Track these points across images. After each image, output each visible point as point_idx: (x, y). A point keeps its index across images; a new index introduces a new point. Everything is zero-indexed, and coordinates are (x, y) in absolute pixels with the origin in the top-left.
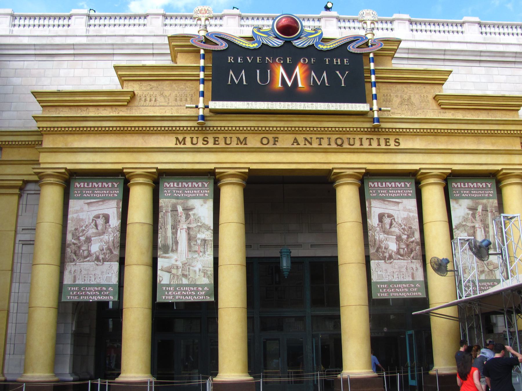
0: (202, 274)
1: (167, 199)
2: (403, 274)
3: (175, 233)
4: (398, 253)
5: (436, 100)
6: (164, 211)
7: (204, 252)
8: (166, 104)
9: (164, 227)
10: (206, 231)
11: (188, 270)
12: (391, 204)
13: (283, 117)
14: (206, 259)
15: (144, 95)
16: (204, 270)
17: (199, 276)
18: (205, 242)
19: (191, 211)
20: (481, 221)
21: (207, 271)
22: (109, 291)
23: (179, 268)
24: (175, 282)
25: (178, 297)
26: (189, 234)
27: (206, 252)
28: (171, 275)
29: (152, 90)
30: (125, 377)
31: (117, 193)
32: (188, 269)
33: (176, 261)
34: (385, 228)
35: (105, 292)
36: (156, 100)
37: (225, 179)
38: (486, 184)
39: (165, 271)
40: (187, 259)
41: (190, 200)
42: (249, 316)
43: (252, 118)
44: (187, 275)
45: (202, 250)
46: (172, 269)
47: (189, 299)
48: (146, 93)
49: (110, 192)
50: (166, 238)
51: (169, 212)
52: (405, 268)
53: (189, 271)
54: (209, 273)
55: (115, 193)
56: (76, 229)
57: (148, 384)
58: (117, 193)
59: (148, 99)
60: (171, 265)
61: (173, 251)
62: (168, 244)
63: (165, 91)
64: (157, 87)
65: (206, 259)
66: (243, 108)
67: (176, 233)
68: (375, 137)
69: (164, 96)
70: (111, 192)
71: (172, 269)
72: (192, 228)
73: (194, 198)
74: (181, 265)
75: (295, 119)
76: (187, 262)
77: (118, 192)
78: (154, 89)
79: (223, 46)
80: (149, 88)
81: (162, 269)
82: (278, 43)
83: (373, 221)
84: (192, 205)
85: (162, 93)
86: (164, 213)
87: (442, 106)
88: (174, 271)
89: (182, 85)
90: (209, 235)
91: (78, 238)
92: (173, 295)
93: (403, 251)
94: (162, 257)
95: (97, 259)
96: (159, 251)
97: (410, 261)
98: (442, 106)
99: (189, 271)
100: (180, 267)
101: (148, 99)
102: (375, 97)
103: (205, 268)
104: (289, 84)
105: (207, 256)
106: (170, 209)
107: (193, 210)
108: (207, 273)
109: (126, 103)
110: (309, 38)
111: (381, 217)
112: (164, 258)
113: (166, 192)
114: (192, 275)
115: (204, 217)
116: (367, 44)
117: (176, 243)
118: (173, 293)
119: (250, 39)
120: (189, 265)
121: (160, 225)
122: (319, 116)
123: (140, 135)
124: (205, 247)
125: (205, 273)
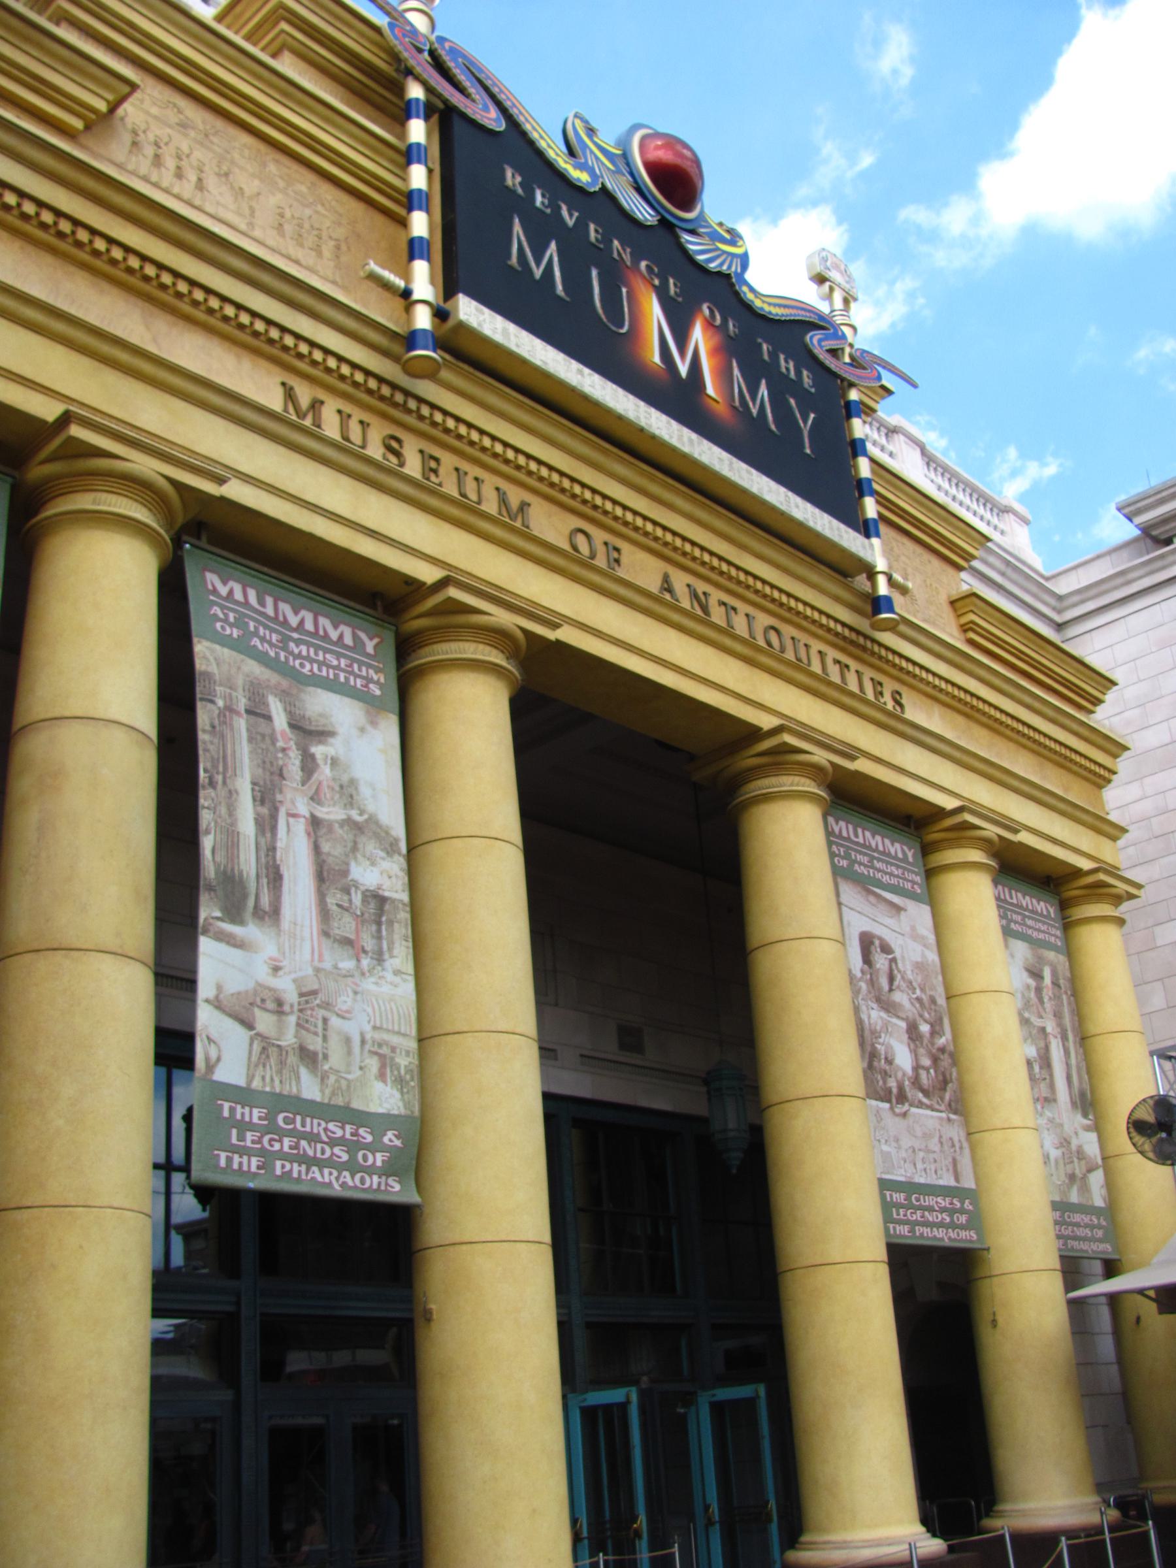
0: (373, 1064)
1: (226, 651)
2: (935, 1161)
3: (267, 825)
4: (916, 1082)
5: (955, 610)
6: (221, 703)
7: (379, 958)
8: (243, 227)
9: (224, 783)
10: (383, 854)
11: (320, 1030)
12: (882, 907)
13: (652, 479)
14: (386, 989)
16: (380, 1045)
17: (361, 1068)
18: (380, 911)
19: (320, 742)
20: (1055, 1016)
21: (393, 1049)
22: (384, 1148)
23: (287, 1008)
24: (265, 1082)
25: (283, 1166)
26: (317, 849)
27: (386, 956)
28: (252, 1040)
30: (844, 1545)
31: (377, 683)
32: (320, 1024)
33: (276, 969)
34: (880, 989)
37: (435, 647)
39: (230, 1015)
40: (317, 970)
41: (311, 689)
42: (163, 1371)
43: (562, 437)
44: (315, 1054)
45: (369, 943)
46: (257, 1011)
47: (324, 1184)
48: (161, 132)
49: (351, 666)
50: (232, 839)
51: (238, 713)
52: (936, 1139)
53: (325, 1038)
54: (403, 1061)
57: (1104, 1534)
58: (377, 683)
59: (170, 163)
60: (251, 985)
61: (259, 914)
62: (241, 873)
63: (237, 170)
65: (386, 989)
66: (568, 380)
67: (274, 829)
69: (232, 188)
71: (257, 1011)
72: (330, 825)
73: (331, 686)
74: (291, 996)
75: (679, 502)
76: (316, 987)
80: (173, 118)
81: (217, 997)
84: (321, 715)
85: (225, 168)
86: (221, 713)
87: (972, 635)
88: (265, 1022)
89: (302, 183)
90: (394, 879)
92: (262, 1153)
93: (928, 1079)
94: (222, 937)
96: (204, 898)
97: (943, 1115)
98: (972, 635)
99: (325, 1038)
100: (292, 1006)
103: (386, 1036)
105: (389, 976)
106: (242, 703)
107: (331, 740)
108: (392, 1059)
109: (78, 124)
110: (717, 249)
112: (228, 943)
113: (221, 616)
114: (336, 1059)
115: (374, 789)
117: (275, 877)
118: (260, 1141)
120: (327, 1006)
121: (209, 765)
122: (741, 521)
123: (133, 299)
124: (379, 931)
125: (382, 1057)
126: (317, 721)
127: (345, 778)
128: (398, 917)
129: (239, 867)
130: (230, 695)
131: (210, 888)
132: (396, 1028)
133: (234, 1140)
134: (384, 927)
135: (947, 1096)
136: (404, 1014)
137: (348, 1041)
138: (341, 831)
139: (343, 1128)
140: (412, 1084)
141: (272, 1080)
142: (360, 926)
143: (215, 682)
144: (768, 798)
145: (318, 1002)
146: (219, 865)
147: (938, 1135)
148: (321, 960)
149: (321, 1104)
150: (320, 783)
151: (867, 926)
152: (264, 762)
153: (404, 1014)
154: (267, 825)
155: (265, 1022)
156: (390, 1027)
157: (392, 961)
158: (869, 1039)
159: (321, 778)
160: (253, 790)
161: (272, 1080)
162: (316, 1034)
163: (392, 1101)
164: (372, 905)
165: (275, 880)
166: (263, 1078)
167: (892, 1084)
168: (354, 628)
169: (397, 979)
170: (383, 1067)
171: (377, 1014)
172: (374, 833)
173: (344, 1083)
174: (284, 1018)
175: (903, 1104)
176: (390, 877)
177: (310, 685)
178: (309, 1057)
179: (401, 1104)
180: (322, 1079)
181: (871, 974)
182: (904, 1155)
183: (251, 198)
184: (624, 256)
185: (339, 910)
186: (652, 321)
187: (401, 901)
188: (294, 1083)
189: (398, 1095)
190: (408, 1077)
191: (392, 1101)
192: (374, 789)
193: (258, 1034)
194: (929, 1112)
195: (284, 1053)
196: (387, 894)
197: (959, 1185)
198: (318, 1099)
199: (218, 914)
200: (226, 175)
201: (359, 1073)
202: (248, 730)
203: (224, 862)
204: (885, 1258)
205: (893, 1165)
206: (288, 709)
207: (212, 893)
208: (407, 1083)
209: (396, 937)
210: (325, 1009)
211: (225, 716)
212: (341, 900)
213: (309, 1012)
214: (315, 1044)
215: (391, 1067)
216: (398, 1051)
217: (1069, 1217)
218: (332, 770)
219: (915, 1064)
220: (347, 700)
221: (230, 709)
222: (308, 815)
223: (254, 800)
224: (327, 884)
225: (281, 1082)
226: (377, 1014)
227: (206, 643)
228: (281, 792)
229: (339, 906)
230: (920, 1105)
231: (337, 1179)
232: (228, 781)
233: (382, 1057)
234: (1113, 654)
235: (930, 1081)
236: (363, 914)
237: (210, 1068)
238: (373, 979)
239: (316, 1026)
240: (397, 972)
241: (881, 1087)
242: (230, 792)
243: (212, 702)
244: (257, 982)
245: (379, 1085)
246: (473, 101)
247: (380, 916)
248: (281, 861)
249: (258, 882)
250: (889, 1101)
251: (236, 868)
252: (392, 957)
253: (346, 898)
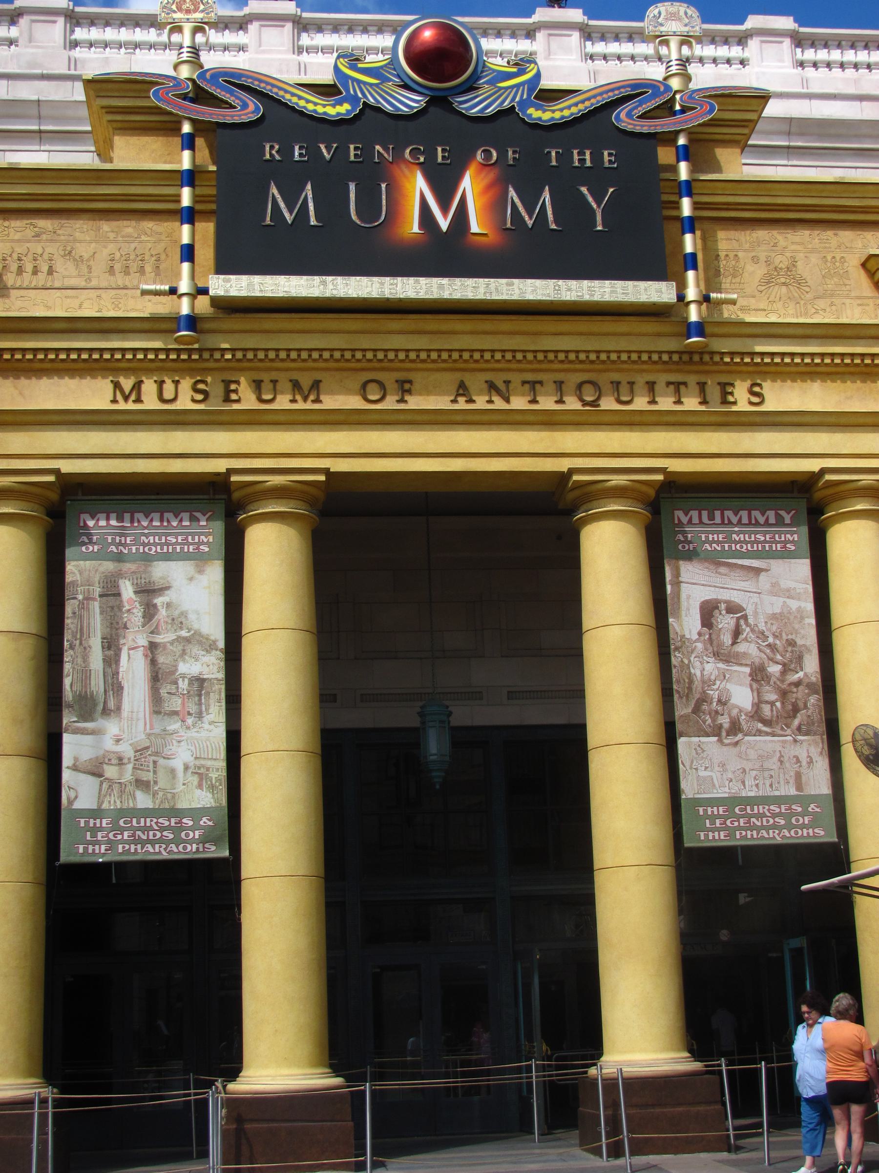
0: (195, 780)
3: (112, 661)
6: (80, 597)
7: (200, 716)
8: (83, 284)
9: (81, 644)
12: (738, 573)
14: (204, 734)
15: (15, 256)
16: (199, 768)
18: (201, 687)
19: (160, 595)
21: (208, 769)
23: (126, 761)
24: (112, 803)
27: (204, 714)
28: (101, 783)
29: (39, 241)
31: (208, 543)
32: (151, 765)
33: (118, 741)
34: (720, 645)
35: (801, 819)
36: (51, 271)
38: (777, 515)
39: (85, 773)
40: (149, 735)
44: (148, 782)
45: (193, 709)
47: (155, 853)
49: (186, 539)
50: (85, 674)
51: (94, 599)
52: (775, 759)
53: (155, 772)
55: (203, 543)
58: (208, 544)
59: (29, 267)
63: (78, 244)
64: (55, 232)
65: (204, 734)
68: (692, 380)
70: (777, 539)
71: (105, 766)
73: (167, 557)
77: (796, 536)
78: (44, 237)
80: (29, 233)
81: (74, 765)
84: (161, 578)
86: (81, 603)
88: (111, 772)
90: (211, 666)
93: (772, 710)
94: (77, 731)
97: (789, 738)
99: (155, 772)
101: (29, 267)
102: (691, 261)
103: (203, 762)
104: (444, 224)
105: (206, 726)
108: (207, 775)
111: (708, 611)
112: (82, 734)
115: (198, 614)
116: (667, 108)
117: (115, 687)
118: (107, 836)
120: (156, 754)
124: (200, 700)
125: (200, 775)
126: (158, 582)
127: (176, 613)
128: (213, 689)
129: (90, 688)
130: (88, 590)
131: (69, 706)
132: (210, 757)
133: (89, 838)
134: (203, 697)
135: (796, 722)
136: (215, 746)
138: (171, 648)
139: (169, 820)
140: (221, 787)
141: (115, 802)
142: (186, 700)
143: (77, 585)
144: (585, 521)
145: (149, 753)
146: (76, 692)
147: (778, 755)
148: (152, 728)
149: (153, 809)
151: (709, 594)
152: (112, 624)
153: (215, 746)
156: (206, 757)
157: (208, 716)
158: (699, 689)
159: (161, 617)
160: (102, 642)
161: (115, 802)
162: (149, 771)
163: (206, 799)
164: (196, 685)
166: (110, 802)
167: (725, 721)
169: (212, 727)
170: (201, 780)
171: (198, 750)
172: (198, 641)
173: (169, 796)
174: (123, 767)
175: (735, 735)
176: (208, 666)
178: (142, 784)
179: (212, 801)
180: (154, 795)
182: (730, 775)
183: (88, 260)
185: (169, 696)
186: (415, 191)
187: (217, 679)
188: (131, 801)
189: (210, 796)
190: (217, 784)
191: (206, 799)
192: (198, 614)
193: (106, 779)
195: (124, 786)
196: (205, 677)
198: (151, 807)
199: (76, 719)
200: (70, 253)
202: (100, 607)
205: (714, 785)
206: (135, 581)
207: (70, 709)
208: (217, 787)
209: (212, 702)
210: (155, 756)
211: (83, 604)
212: (171, 689)
213: (143, 760)
214: (147, 776)
215: (206, 779)
216: (211, 769)
218: (166, 611)
219: (756, 700)
220: (181, 563)
221: (88, 599)
222: (146, 644)
223: (103, 647)
224: (161, 681)
225: (121, 802)
226: (198, 750)
227: (73, 563)
228: (124, 637)
229: (169, 693)
230: (759, 733)
231: (165, 849)
232: (83, 642)
233: (200, 775)
235: (775, 713)
236: (189, 692)
237: (70, 802)
238: (195, 730)
239: (148, 766)
240: (211, 723)
241: (709, 725)
242: (85, 648)
244: (105, 750)
246: (232, 107)
247: (201, 691)
248: (123, 678)
249: (105, 694)
251: (88, 690)
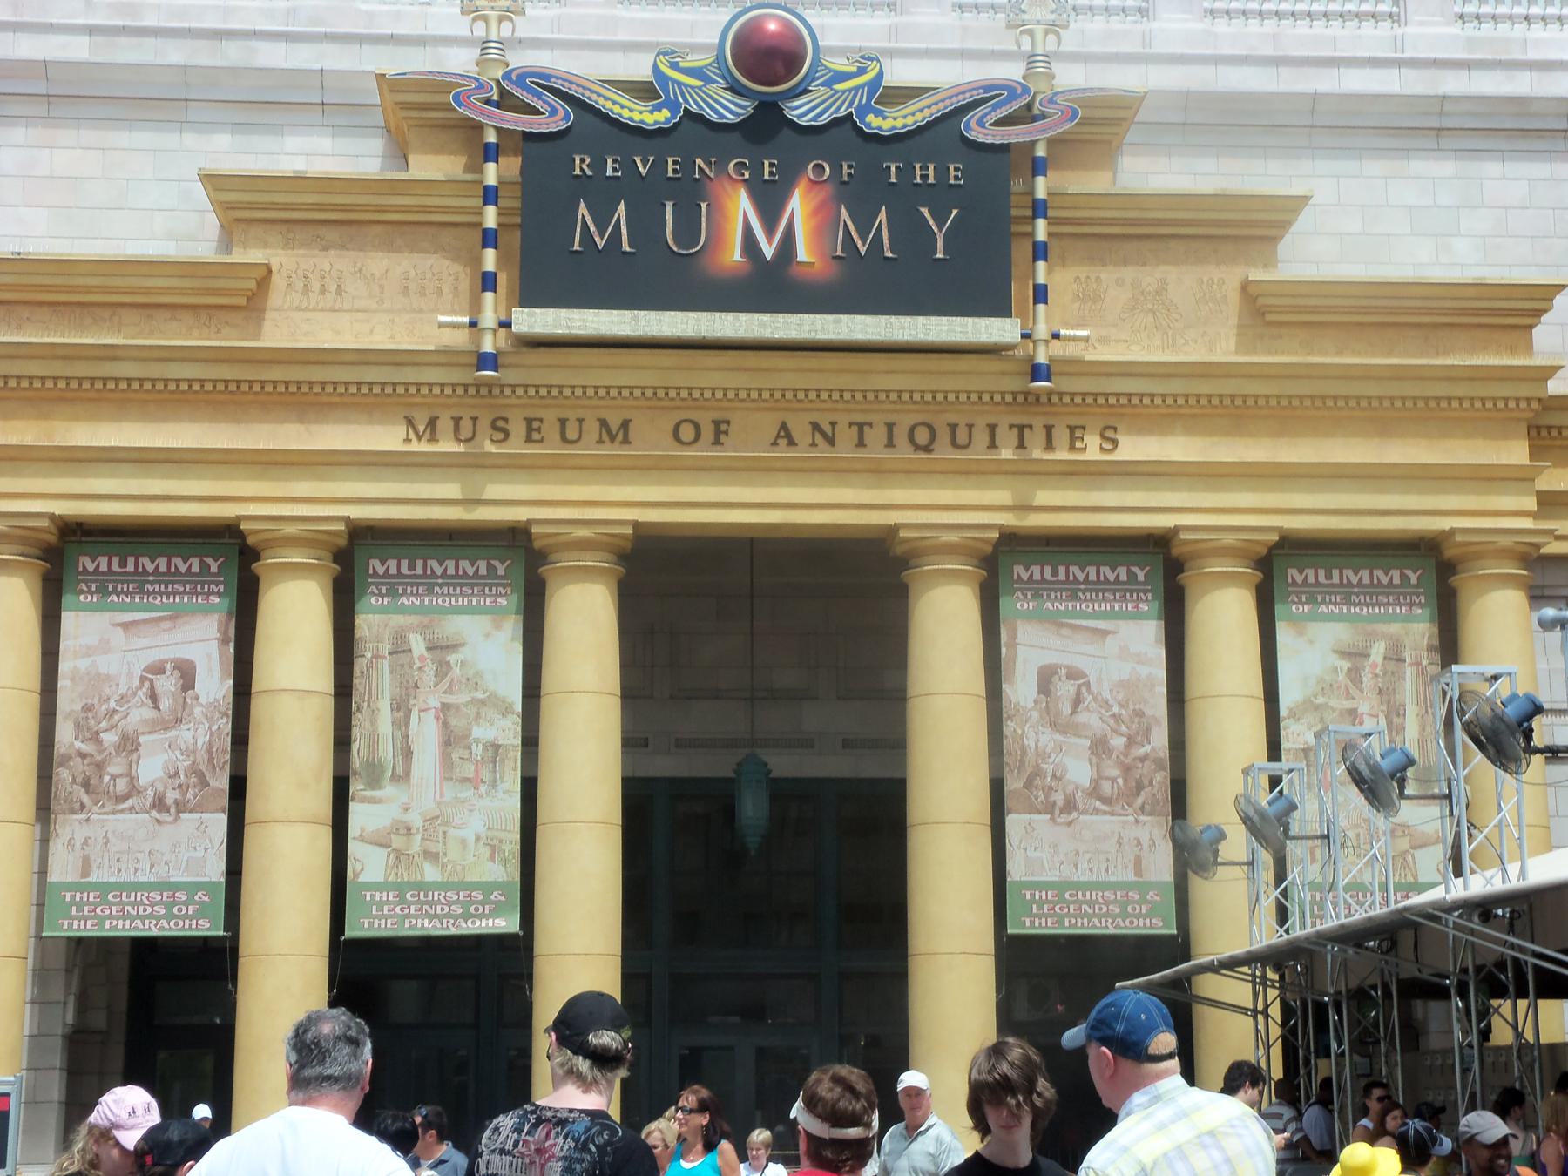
0: (487, 852)
2: (1108, 860)
3: (402, 724)
7: (494, 784)
9: (369, 706)
11: (440, 839)
16: (492, 840)
18: (496, 753)
21: (501, 841)
23: (414, 831)
27: (498, 782)
39: (371, 843)
40: (439, 804)
50: (374, 741)
51: (383, 657)
56: (87, 708)
67: (407, 724)
76: (437, 813)
79: (553, 119)
82: (728, 108)
83: (1021, 690)
91: (95, 738)
95: (159, 804)
97: (1131, 818)
104: (769, 251)
108: (499, 847)
110: (837, 92)
111: (1046, 678)
114: (453, 853)
117: (407, 753)
119: (644, 91)
120: (446, 823)
125: (493, 848)
135: (1140, 801)
137: (463, 842)
141: (402, 874)
150: (452, 680)
154: (402, 724)
155: (397, 842)
165: (407, 756)
168: (488, 560)
177: (447, 614)
180: (442, 868)
181: (1047, 702)
184: (707, 171)
194: (1108, 818)
196: (500, 743)
197: (1141, 880)
199: (362, 787)
201: (473, 859)
203: (367, 754)
204: (993, 952)
217: (614, 1039)
230: (1097, 811)
234: (752, 626)
243: (364, 656)
245: (490, 864)
250: (1052, 813)
252: (502, 782)
253: (467, 752)
